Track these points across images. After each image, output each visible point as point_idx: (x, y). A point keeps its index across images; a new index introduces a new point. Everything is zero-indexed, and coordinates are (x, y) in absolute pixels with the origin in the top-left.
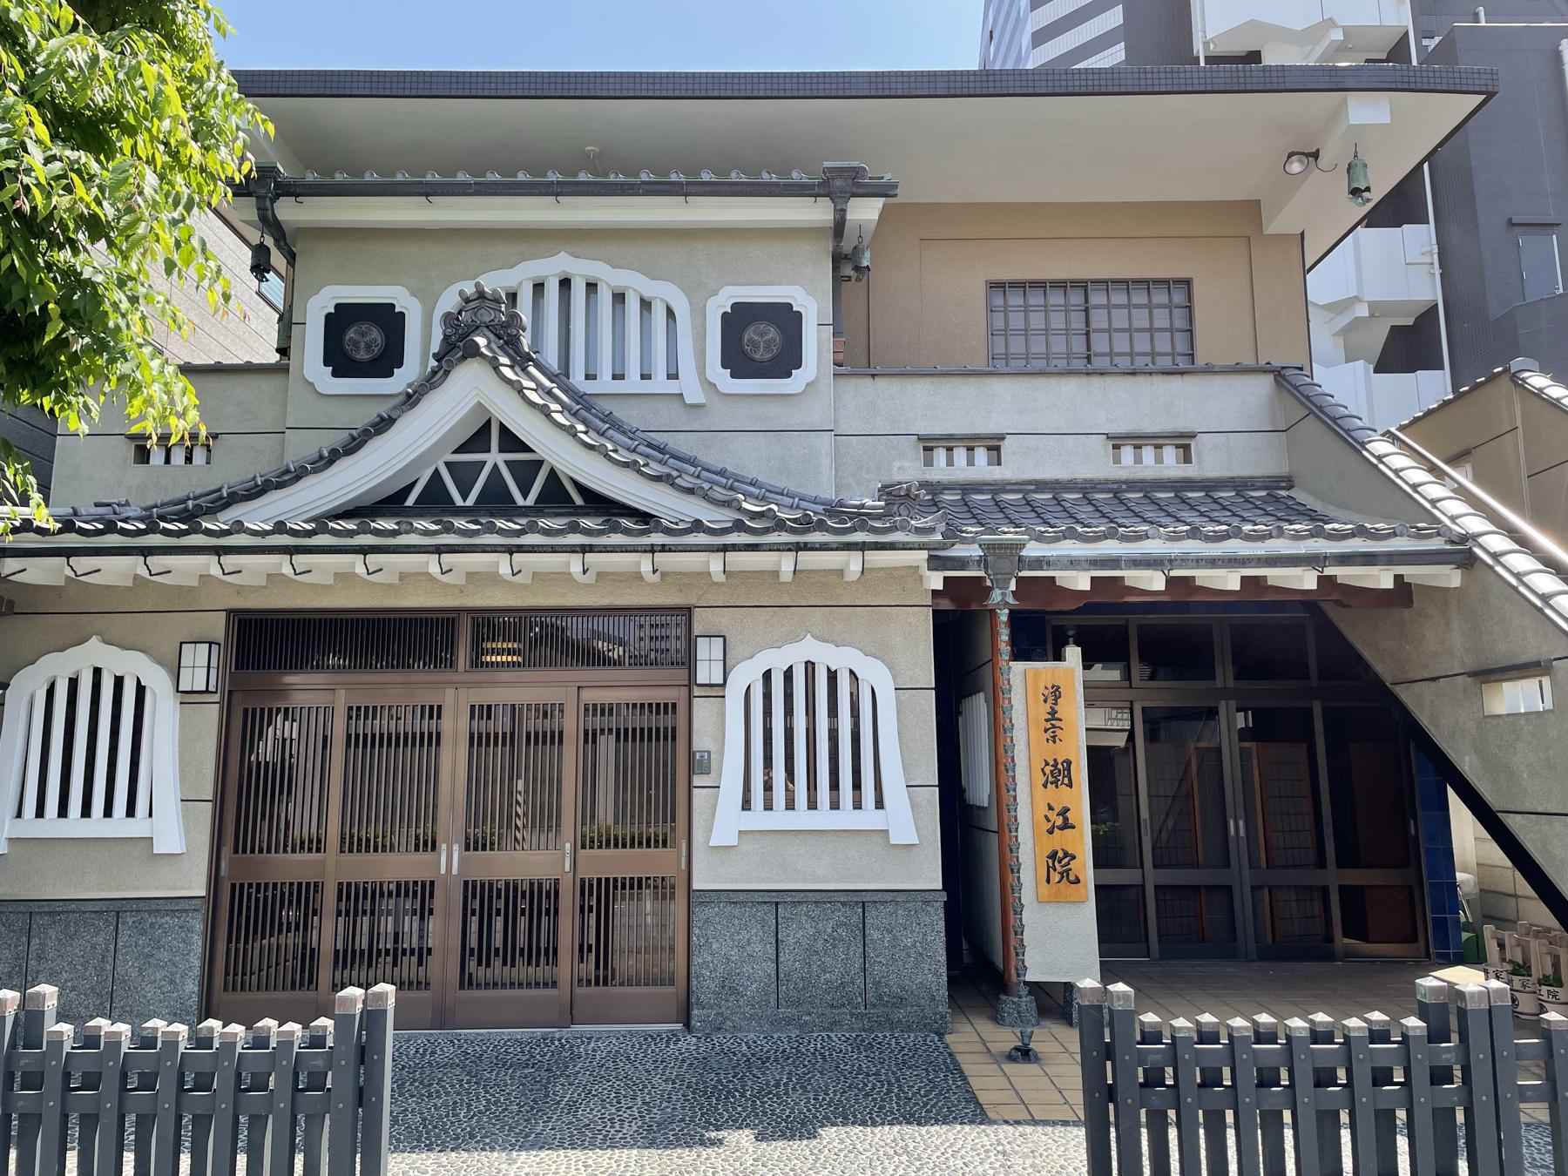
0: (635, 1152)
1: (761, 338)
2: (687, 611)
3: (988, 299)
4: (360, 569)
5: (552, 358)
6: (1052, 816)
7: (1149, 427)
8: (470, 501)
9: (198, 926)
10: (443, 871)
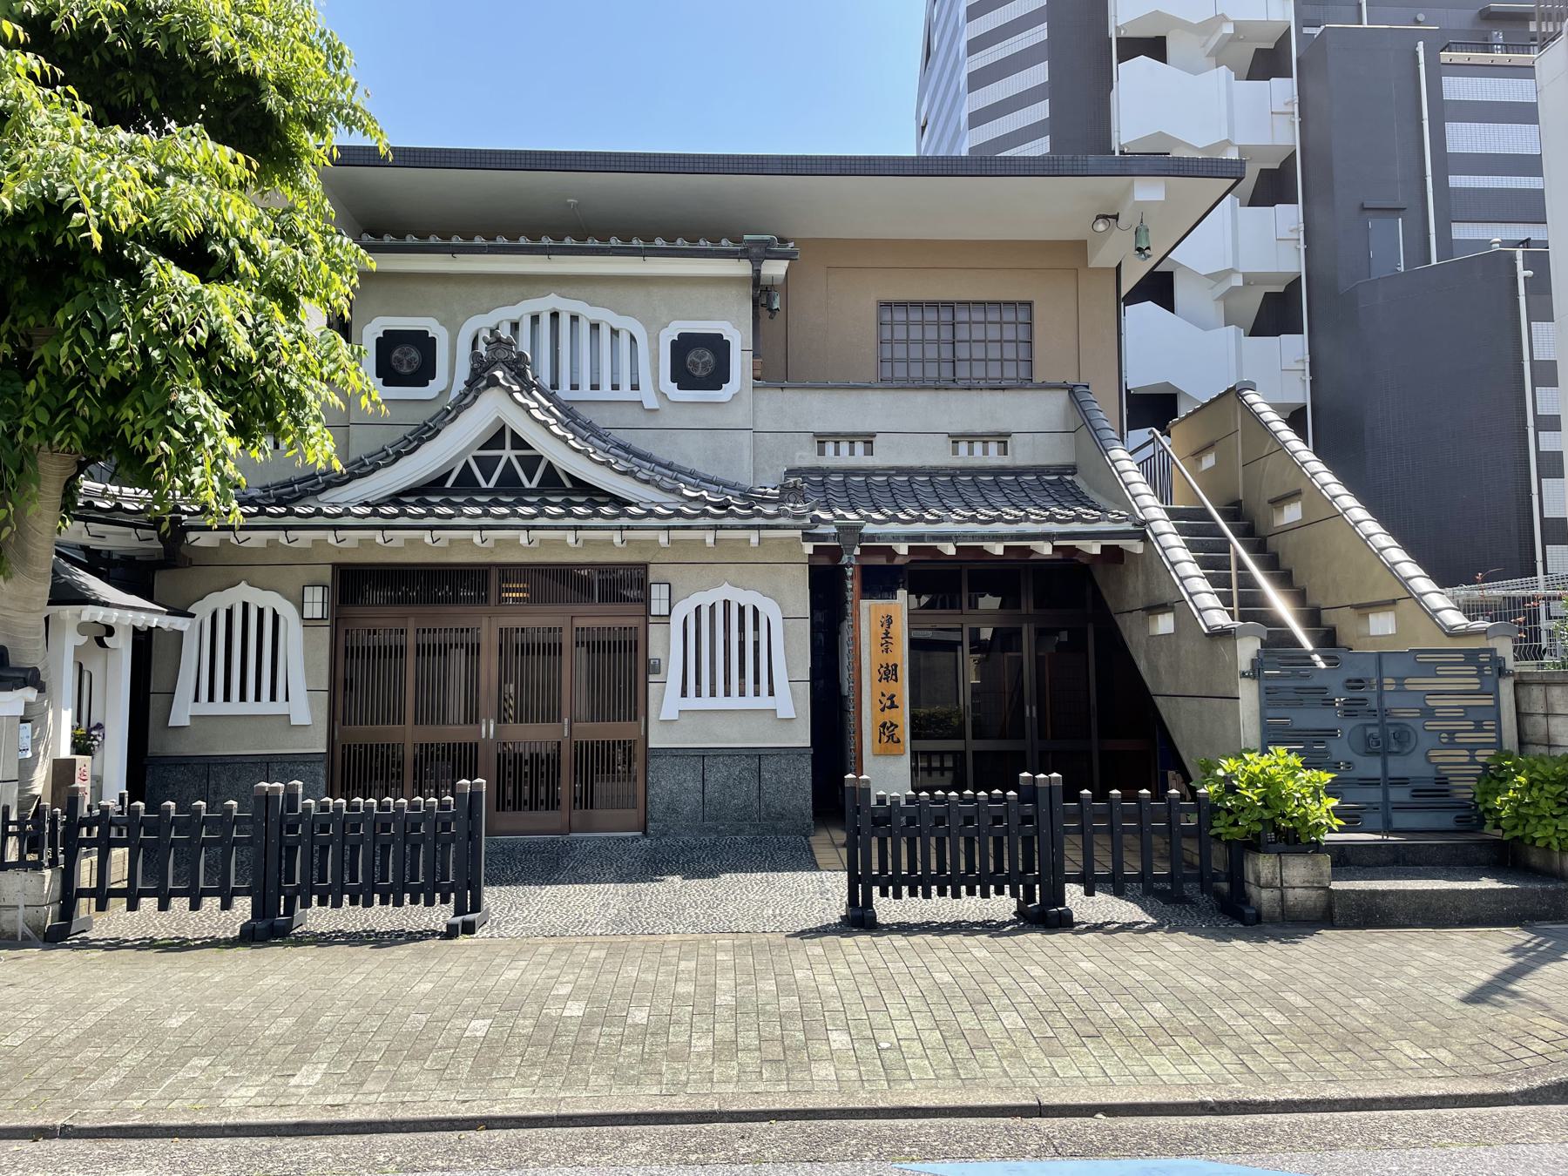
0: (612, 885)
1: (701, 360)
2: (645, 566)
3: (879, 316)
4: (428, 540)
5: (546, 380)
6: (884, 700)
7: (979, 429)
8: (492, 484)
9: (323, 772)
10: (483, 737)
